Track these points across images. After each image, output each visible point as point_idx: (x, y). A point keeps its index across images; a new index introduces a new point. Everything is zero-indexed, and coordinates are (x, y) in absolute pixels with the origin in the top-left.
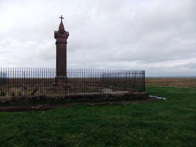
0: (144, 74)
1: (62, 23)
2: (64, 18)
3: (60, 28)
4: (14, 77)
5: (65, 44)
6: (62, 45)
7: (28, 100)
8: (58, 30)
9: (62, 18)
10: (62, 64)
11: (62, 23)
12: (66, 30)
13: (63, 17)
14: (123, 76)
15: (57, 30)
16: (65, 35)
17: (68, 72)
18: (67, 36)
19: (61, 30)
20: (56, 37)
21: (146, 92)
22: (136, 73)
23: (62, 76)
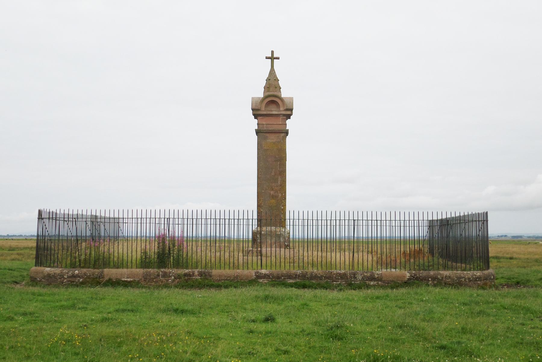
0: (487, 221)
1: (272, 72)
2: (278, 58)
3: (267, 88)
4: (310, 236)
5: (283, 135)
6: (272, 138)
7: (175, 278)
8: (261, 95)
9: (272, 58)
10: (272, 192)
11: (272, 72)
12: (285, 94)
13: (275, 56)
14: (211, 231)
15: (260, 94)
16: (282, 109)
17: (287, 217)
18: (289, 113)
19: (269, 96)
20: (256, 116)
21: (490, 271)
22: (403, 224)
23: (273, 228)
